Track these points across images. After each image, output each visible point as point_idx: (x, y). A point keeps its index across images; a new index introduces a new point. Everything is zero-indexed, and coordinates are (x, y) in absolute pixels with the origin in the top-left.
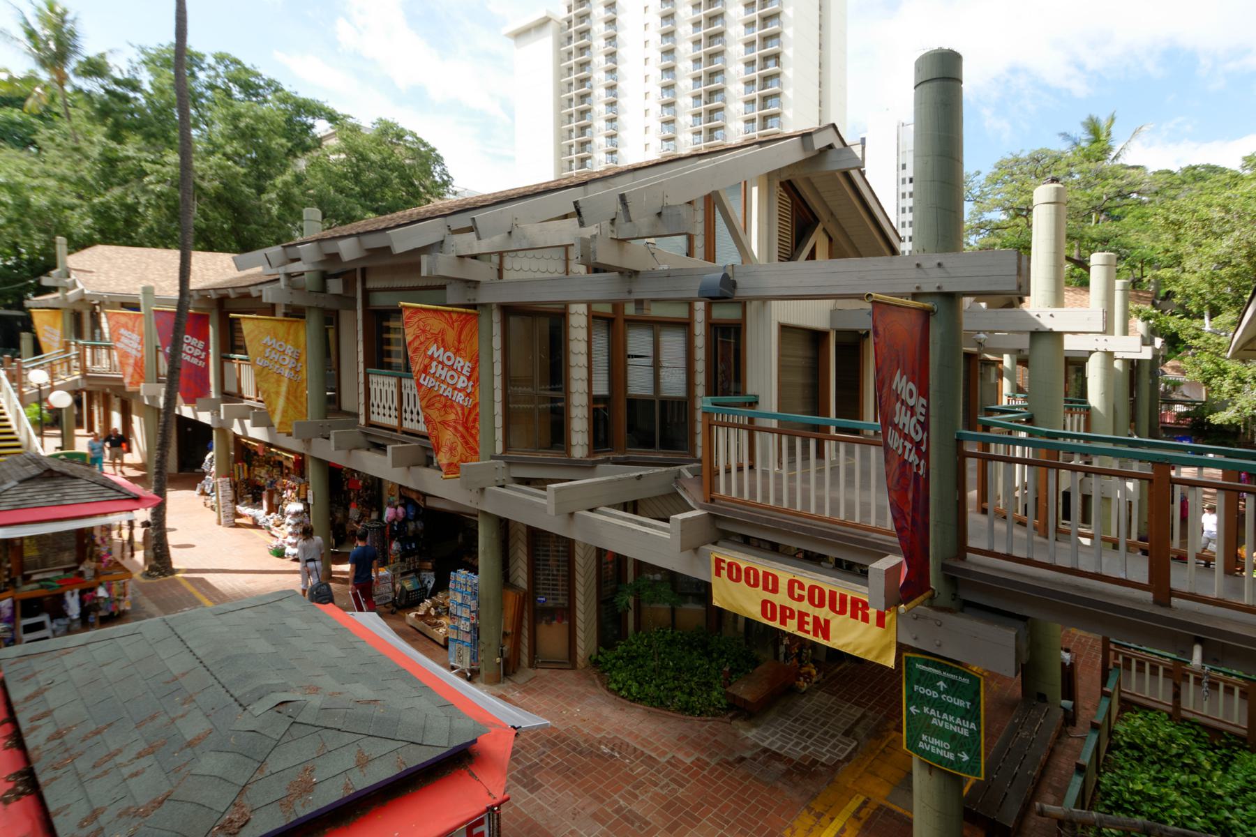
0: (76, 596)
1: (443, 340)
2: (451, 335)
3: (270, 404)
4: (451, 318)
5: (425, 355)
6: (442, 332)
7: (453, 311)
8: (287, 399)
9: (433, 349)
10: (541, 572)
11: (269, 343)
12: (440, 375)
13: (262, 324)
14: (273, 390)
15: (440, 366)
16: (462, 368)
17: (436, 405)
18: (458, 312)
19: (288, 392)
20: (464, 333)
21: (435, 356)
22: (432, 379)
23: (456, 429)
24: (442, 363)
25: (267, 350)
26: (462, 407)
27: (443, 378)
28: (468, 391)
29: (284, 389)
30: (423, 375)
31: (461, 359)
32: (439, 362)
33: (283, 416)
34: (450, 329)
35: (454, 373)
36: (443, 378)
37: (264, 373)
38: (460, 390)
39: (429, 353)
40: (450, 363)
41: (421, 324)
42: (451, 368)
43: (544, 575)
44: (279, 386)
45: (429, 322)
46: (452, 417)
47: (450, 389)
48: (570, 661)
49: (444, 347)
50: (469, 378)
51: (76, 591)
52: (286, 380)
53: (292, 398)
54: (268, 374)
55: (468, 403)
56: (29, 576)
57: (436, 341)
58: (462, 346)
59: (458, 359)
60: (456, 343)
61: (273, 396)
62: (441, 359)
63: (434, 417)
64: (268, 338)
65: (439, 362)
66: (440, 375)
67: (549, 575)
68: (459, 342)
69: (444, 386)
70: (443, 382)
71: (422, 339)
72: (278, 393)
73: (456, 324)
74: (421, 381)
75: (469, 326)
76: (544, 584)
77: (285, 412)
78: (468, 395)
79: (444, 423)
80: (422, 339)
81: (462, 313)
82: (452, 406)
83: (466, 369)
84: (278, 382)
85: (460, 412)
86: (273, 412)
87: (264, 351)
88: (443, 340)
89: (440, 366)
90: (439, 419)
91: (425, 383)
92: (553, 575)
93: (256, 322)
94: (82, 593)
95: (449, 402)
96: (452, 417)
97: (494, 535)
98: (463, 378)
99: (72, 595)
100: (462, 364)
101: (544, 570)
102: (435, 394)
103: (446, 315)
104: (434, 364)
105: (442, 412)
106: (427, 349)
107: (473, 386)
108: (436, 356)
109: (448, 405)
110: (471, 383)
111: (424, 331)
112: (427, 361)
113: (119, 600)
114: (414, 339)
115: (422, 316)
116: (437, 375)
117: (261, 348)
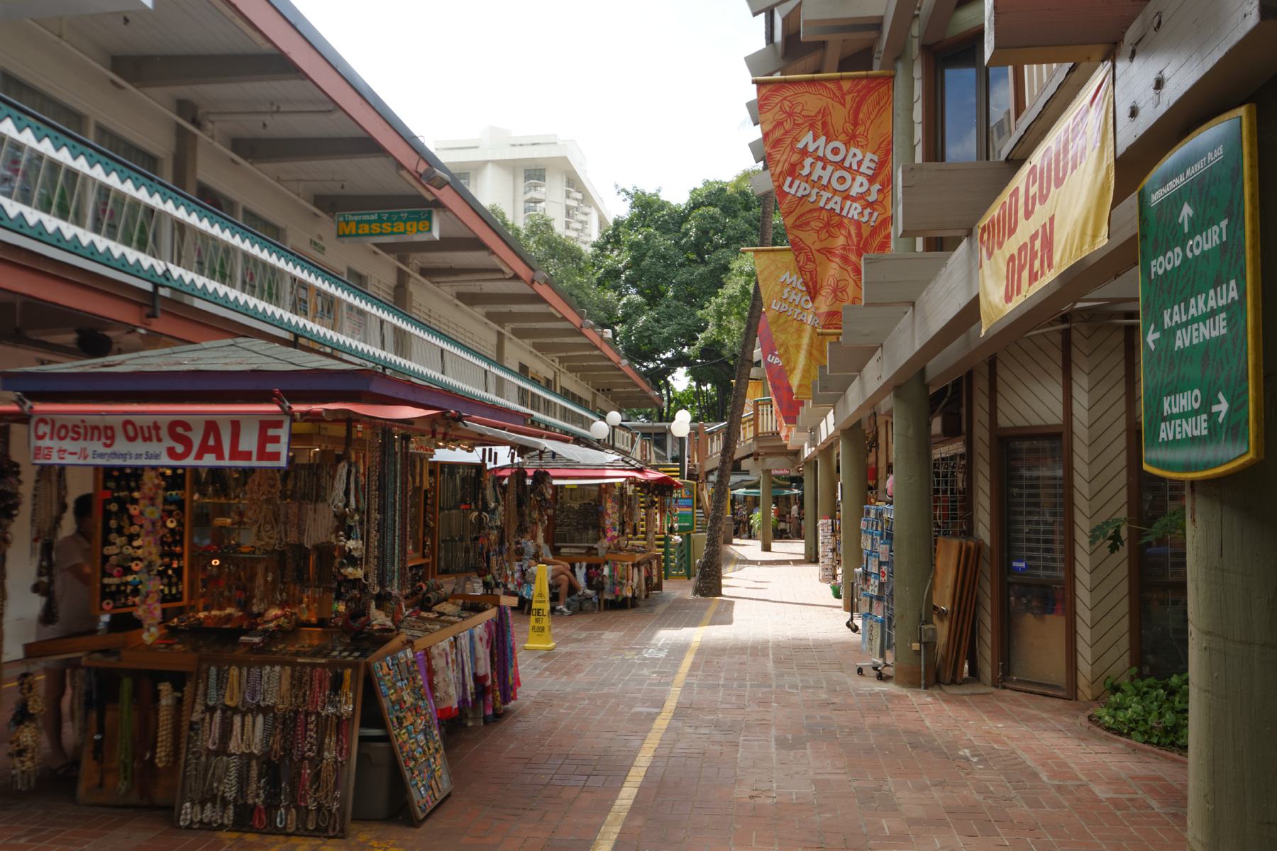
0: (584, 569)
1: (825, 125)
2: (839, 116)
3: (788, 361)
4: (840, 88)
5: (793, 149)
6: (824, 112)
7: (841, 78)
8: (810, 354)
9: (807, 139)
10: (1024, 518)
11: (788, 281)
12: (820, 178)
13: (779, 256)
14: (792, 343)
15: (820, 164)
16: (860, 163)
17: (812, 224)
18: (853, 78)
19: (811, 345)
20: (864, 109)
21: (811, 149)
22: (803, 185)
23: (845, 259)
24: (823, 159)
25: (786, 291)
26: (858, 225)
27: (824, 182)
28: (871, 199)
29: (805, 341)
30: (789, 180)
31: (858, 152)
32: (819, 158)
33: (803, 377)
34: (837, 105)
35: (844, 173)
36: (824, 182)
37: (782, 321)
38: (854, 199)
39: (800, 145)
40: (838, 158)
41: (786, 104)
42: (840, 165)
43: (1029, 522)
44: (800, 337)
45: (800, 100)
46: (841, 241)
47: (837, 198)
48: (1069, 692)
49: (827, 134)
50: (871, 180)
51: (584, 564)
52: (808, 328)
53: (815, 352)
54: (786, 322)
55: (870, 218)
56: (559, 548)
57: (812, 126)
58: (861, 129)
59: (853, 150)
60: (849, 127)
61: (792, 350)
62: (820, 153)
63: (809, 241)
64: (787, 275)
65: (819, 158)
66: (820, 178)
67: (1038, 523)
68: (855, 124)
69: (826, 195)
70: (825, 188)
71: (788, 126)
72: (798, 347)
73: (848, 98)
74: (786, 188)
75: (872, 99)
76: (1029, 540)
77: (806, 371)
78: (870, 205)
79: (827, 252)
80: (788, 126)
81: (860, 78)
82: (840, 225)
83: (866, 163)
84: (799, 332)
85: (853, 232)
86: (792, 370)
87: (782, 292)
88: (825, 125)
89: (820, 164)
90: (818, 245)
91: (793, 191)
92: (1045, 523)
93: (772, 254)
94: (589, 567)
95: (836, 219)
96: (841, 241)
97: (911, 432)
98: (860, 179)
99: (581, 568)
100: (859, 157)
101: (1029, 513)
102: (810, 207)
103: (831, 86)
104: (808, 161)
105: (824, 235)
106: (797, 140)
107: (879, 191)
108: (811, 148)
109: (833, 222)
110: (877, 186)
111: (790, 114)
112: (795, 158)
113: (621, 583)
114: (775, 127)
115: (788, 92)
116: (814, 177)
117: (777, 288)
